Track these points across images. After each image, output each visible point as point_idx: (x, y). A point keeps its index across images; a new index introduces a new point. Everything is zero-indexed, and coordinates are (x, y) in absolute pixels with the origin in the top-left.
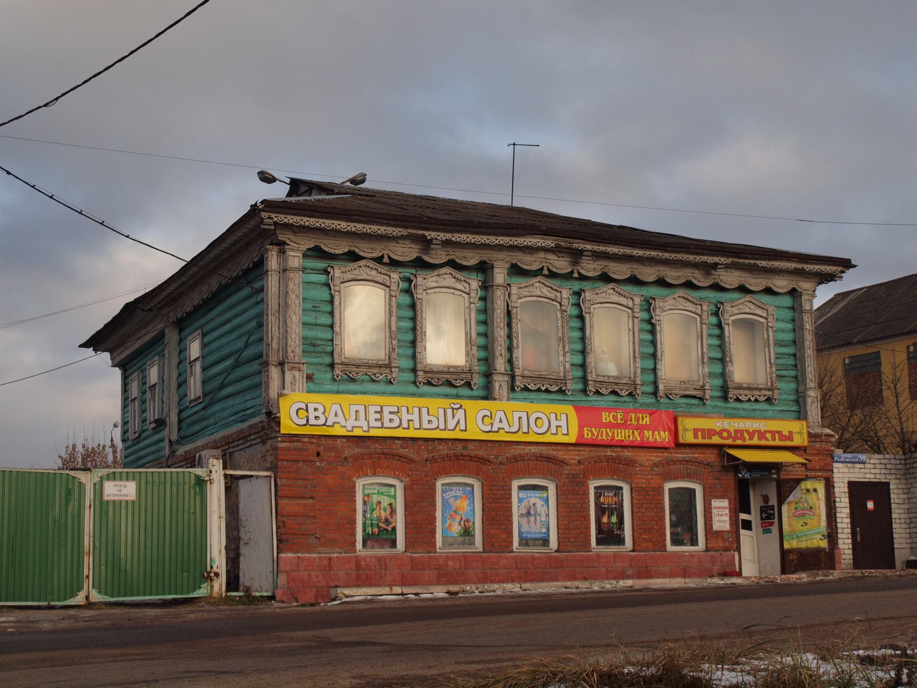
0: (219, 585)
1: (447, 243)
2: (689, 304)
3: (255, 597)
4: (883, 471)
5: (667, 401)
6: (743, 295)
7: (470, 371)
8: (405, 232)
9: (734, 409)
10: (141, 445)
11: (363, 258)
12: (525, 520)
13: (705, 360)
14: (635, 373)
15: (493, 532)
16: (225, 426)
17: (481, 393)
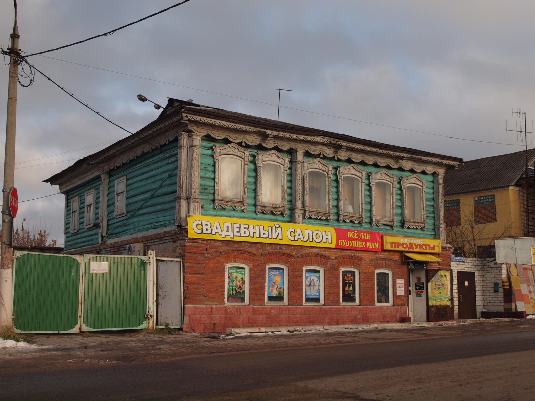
0: (152, 322)
1: (276, 137)
2: (387, 177)
3: (171, 329)
4: (472, 267)
5: (376, 227)
6: (411, 174)
7: (283, 207)
8: (256, 129)
9: (406, 232)
10: (79, 236)
11: (231, 142)
12: (308, 288)
13: (394, 206)
14: (362, 212)
15: (293, 294)
16: (141, 230)
17: (288, 219)
